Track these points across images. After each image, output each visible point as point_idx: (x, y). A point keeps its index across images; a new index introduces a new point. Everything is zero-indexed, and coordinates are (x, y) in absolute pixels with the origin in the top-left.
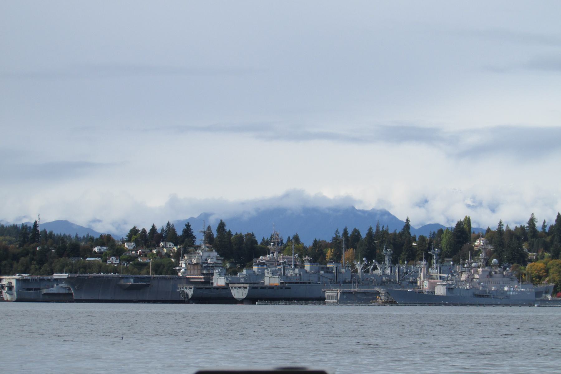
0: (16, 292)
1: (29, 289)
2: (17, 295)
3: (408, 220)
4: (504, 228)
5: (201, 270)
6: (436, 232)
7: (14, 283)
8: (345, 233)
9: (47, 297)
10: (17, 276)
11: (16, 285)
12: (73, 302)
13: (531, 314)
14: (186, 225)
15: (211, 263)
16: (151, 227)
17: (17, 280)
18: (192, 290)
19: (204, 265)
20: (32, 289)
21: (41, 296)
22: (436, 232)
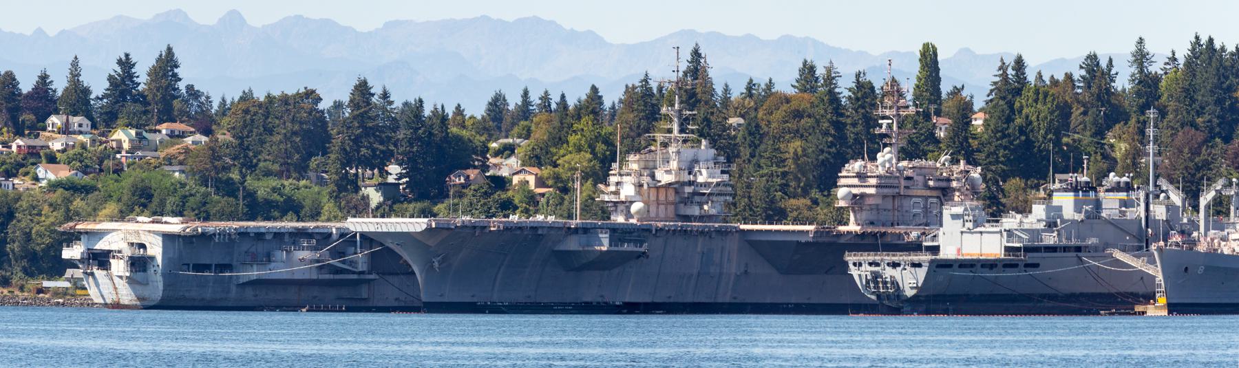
0: (163, 275)
1: (199, 267)
2: (166, 286)
3: (929, 59)
4: (654, 86)
5: (675, 204)
6: (612, 97)
7: (155, 249)
8: (546, 98)
9: (249, 293)
10: (174, 225)
11: (164, 253)
12: (417, 310)
13: (730, 350)
14: (120, 62)
15: (706, 185)
16: (115, 68)
17: (168, 238)
18: (922, 273)
19: (688, 190)
20: (206, 267)
21: (234, 289)
22: (612, 97)
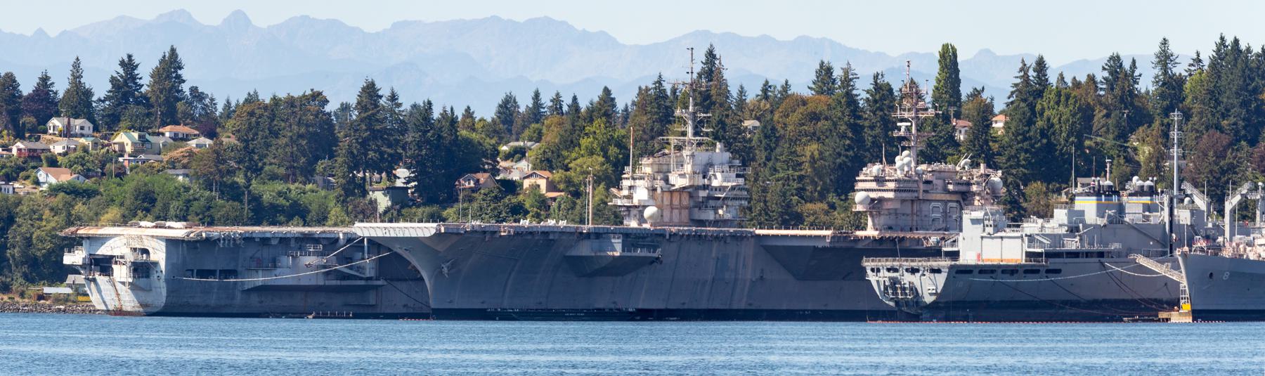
0: (167, 281)
1: (203, 273)
2: (169, 292)
3: (949, 60)
4: (668, 88)
5: (689, 209)
6: (624, 99)
7: (159, 255)
8: (557, 100)
9: (254, 300)
10: (178, 230)
11: (168, 258)
12: (425, 316)
13: (745, 357)
14: (122, 63)
15: (721, 189)
16: (117, 70)
17: (172, 243)
19: (703, 194)
20: (211, 273)
21: (239, 295)
22: (624, 99)
